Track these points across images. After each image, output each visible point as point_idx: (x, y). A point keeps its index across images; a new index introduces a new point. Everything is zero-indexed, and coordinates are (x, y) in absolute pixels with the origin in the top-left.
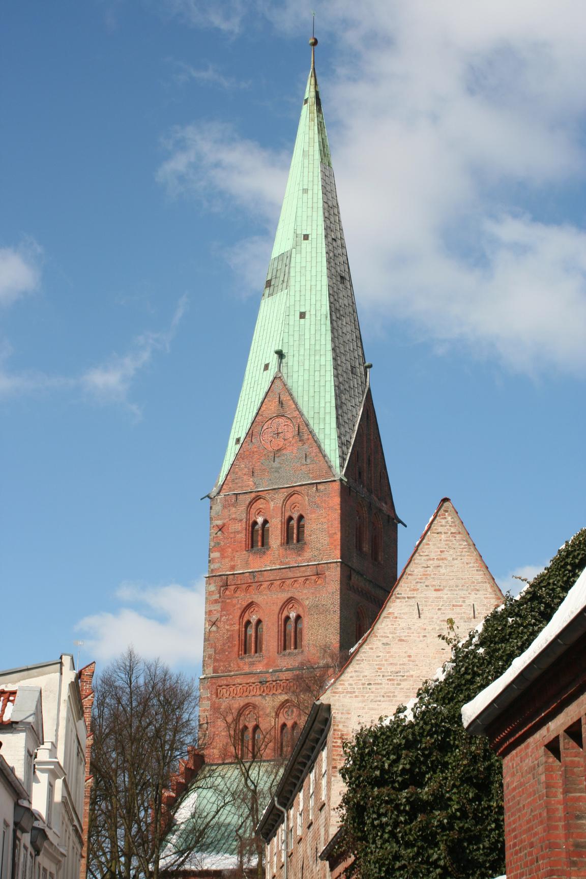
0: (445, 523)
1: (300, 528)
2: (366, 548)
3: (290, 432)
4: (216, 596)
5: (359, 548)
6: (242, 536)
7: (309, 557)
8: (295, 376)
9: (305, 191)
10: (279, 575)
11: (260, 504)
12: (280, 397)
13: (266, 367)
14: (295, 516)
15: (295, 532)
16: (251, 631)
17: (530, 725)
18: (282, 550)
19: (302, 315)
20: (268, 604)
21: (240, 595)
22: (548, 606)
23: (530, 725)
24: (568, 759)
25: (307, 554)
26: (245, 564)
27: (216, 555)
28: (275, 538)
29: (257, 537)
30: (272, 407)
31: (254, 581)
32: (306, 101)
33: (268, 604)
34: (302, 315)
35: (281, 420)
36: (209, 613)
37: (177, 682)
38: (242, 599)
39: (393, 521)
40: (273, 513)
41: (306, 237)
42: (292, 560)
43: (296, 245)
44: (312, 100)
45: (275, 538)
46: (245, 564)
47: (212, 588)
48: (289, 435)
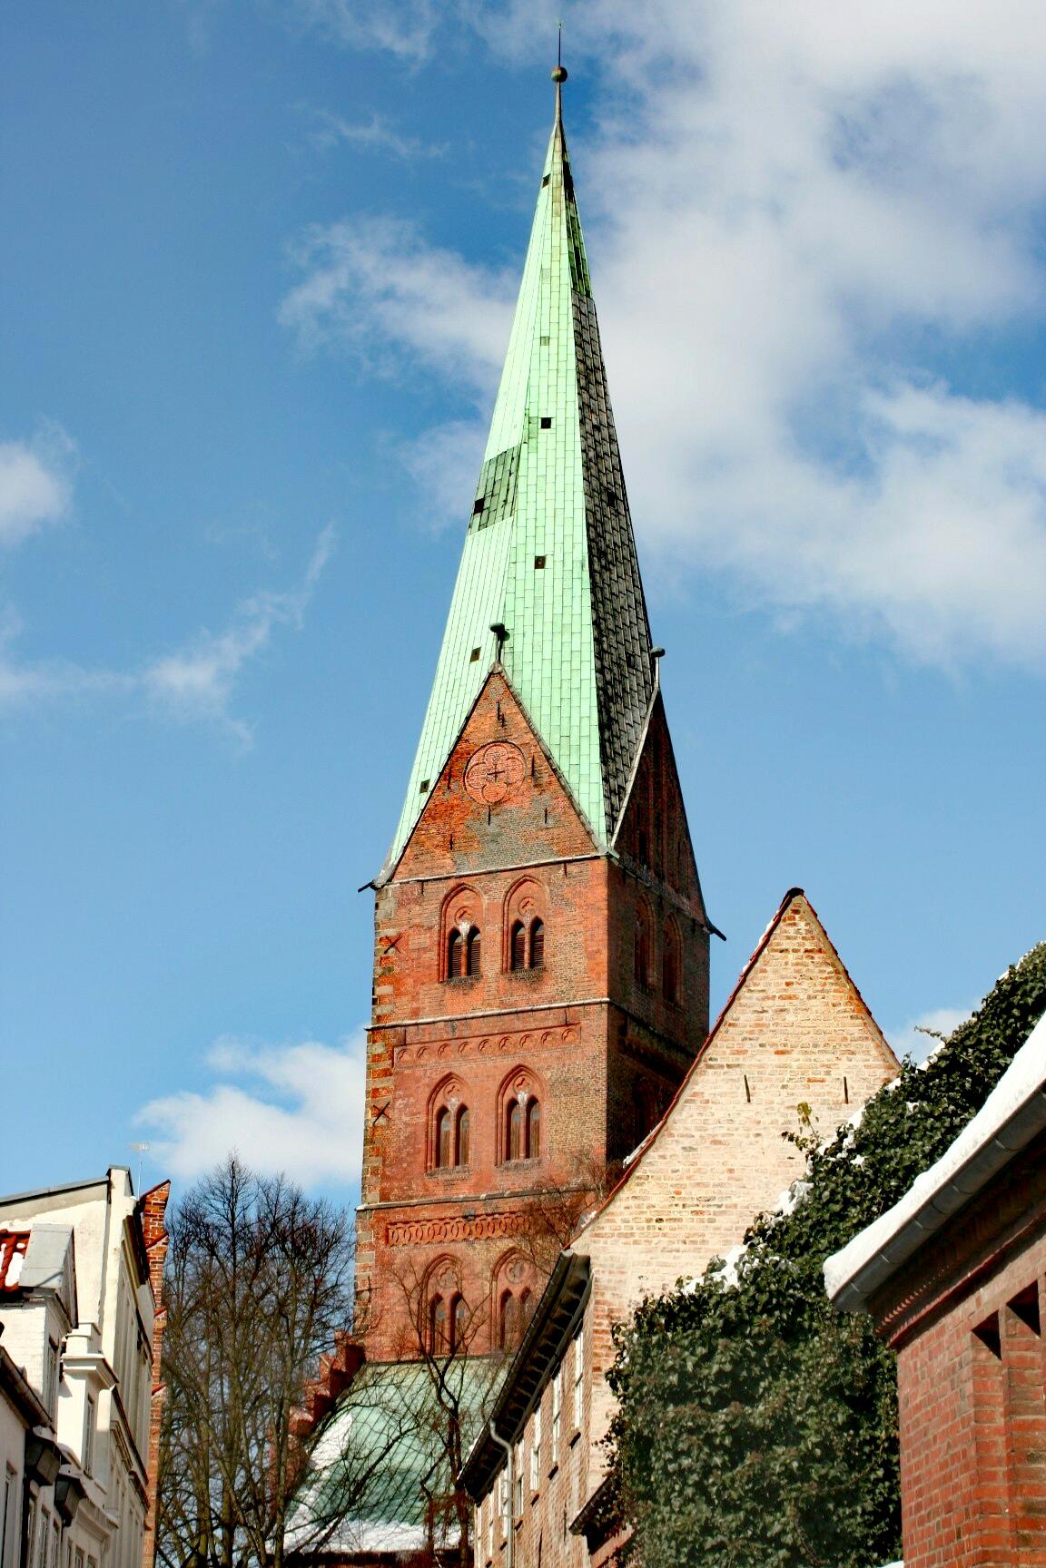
1: (536, 941)
6: (432, 957)
11: (464, 899)
13: (476, 654)
14: (527, 921)
15: (526, 950)
19: (540, 562)
25: (549, 989)
29: (458, 959)
32: (546, 180)
34: (540, 562)
35: (503, 750)
40: (487, 916)
42: (522, 998)
44: (557, 179)
48: (516, 776)
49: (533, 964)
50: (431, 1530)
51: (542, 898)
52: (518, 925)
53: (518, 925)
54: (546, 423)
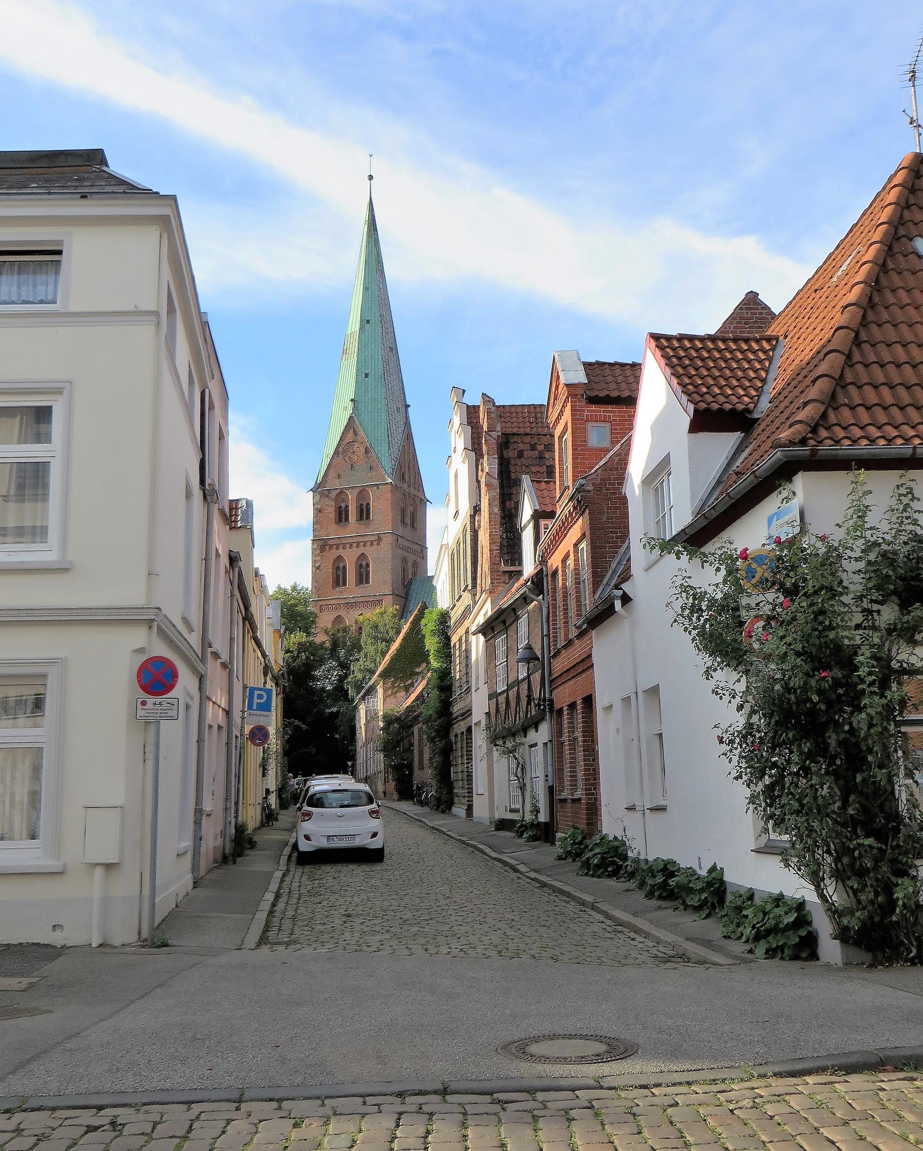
2: (408, 521)
4: (318, 552)
5: (403, 522)
6: (333, 516)
7: (372, 531)
8: (363, 416)
10: (356, 540)
15: (364, 513)
16: (340, 573)
18: (357, 524)
20: (350, 558)
21: (334, 551)
22: (577, 450)
24: (764, 404)
26: (334, 532)
28: (352, 517)
29: (342, 516)
33: (350, 558)
36: (314, 562)
38: (335, 553)
39: (423, 502)
41: (368, 322)
45: (352, 517)
46: (334, 532)
47: (315, 546)
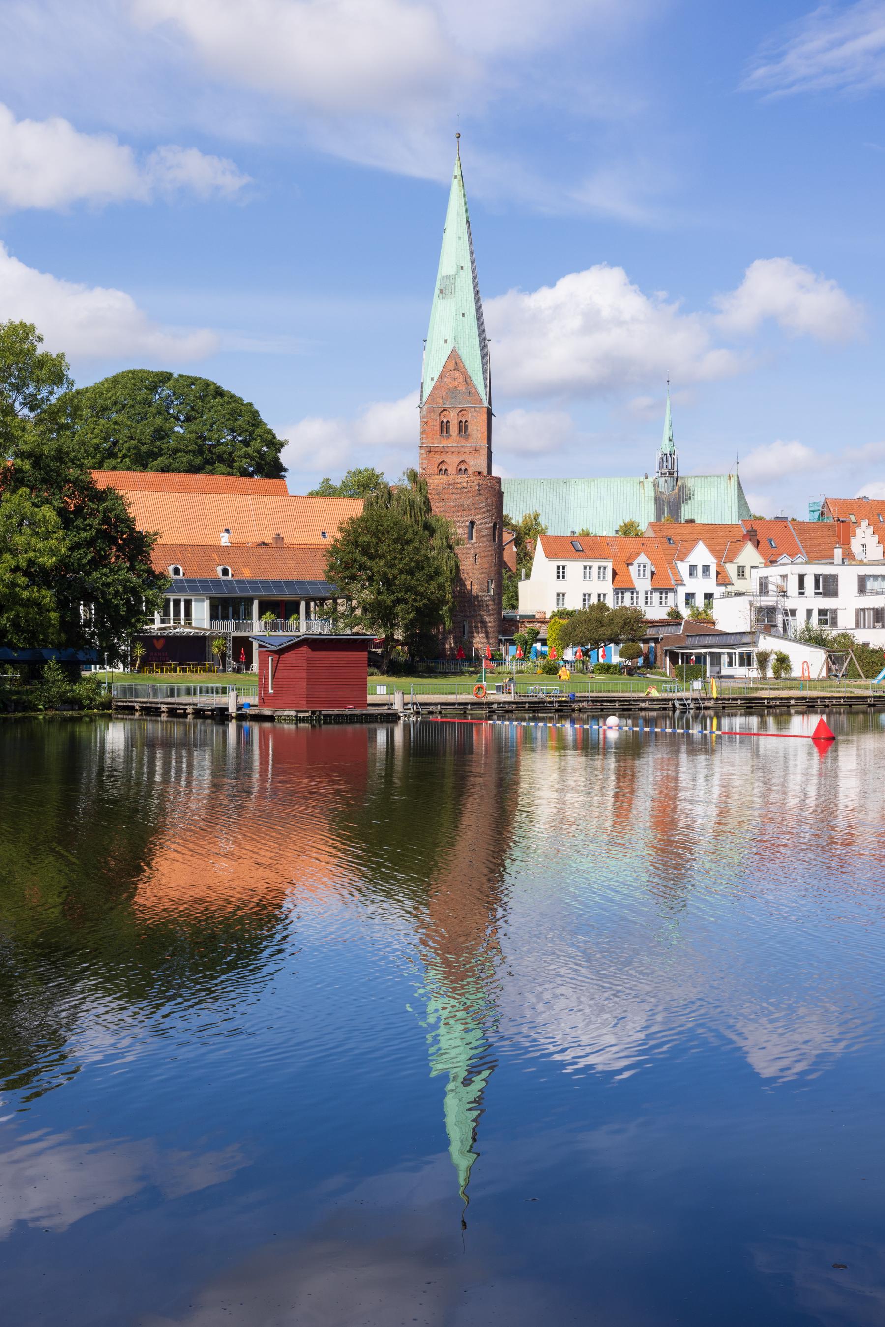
0: (476, 1156)
1: (466, 426)
3: (461, 379)
6: (437, 428)
9: (460, 238)
10: (457, 449)
11: (445, 413)
12: (455, 362)
13: (446, 341)
14: (463, 421)
15: (463, 428)
17: (271, 756)
19: (463, 315)
23: (271, 756)
25: (471, 440)
27: (424, 436)
29: (444, 427)
30: (452, 365)
31: (444, 451)
32: (456, 177)
34: (463, 315)
35: (456, 372)
37: (766, 820)
38: (438, 458)
40: (453, 418)
42: (463, 443)
43: (458, 272)
44: (459, 177)
48: (460, 380)
49: (590, 577)
50: (51, 504)
51: (470, 416)
52: (461, 422)
53: (461, 422)
54: (462, 268)
